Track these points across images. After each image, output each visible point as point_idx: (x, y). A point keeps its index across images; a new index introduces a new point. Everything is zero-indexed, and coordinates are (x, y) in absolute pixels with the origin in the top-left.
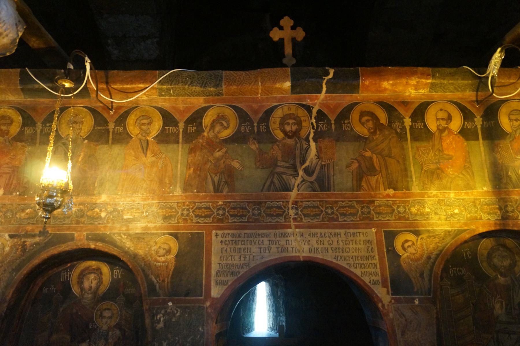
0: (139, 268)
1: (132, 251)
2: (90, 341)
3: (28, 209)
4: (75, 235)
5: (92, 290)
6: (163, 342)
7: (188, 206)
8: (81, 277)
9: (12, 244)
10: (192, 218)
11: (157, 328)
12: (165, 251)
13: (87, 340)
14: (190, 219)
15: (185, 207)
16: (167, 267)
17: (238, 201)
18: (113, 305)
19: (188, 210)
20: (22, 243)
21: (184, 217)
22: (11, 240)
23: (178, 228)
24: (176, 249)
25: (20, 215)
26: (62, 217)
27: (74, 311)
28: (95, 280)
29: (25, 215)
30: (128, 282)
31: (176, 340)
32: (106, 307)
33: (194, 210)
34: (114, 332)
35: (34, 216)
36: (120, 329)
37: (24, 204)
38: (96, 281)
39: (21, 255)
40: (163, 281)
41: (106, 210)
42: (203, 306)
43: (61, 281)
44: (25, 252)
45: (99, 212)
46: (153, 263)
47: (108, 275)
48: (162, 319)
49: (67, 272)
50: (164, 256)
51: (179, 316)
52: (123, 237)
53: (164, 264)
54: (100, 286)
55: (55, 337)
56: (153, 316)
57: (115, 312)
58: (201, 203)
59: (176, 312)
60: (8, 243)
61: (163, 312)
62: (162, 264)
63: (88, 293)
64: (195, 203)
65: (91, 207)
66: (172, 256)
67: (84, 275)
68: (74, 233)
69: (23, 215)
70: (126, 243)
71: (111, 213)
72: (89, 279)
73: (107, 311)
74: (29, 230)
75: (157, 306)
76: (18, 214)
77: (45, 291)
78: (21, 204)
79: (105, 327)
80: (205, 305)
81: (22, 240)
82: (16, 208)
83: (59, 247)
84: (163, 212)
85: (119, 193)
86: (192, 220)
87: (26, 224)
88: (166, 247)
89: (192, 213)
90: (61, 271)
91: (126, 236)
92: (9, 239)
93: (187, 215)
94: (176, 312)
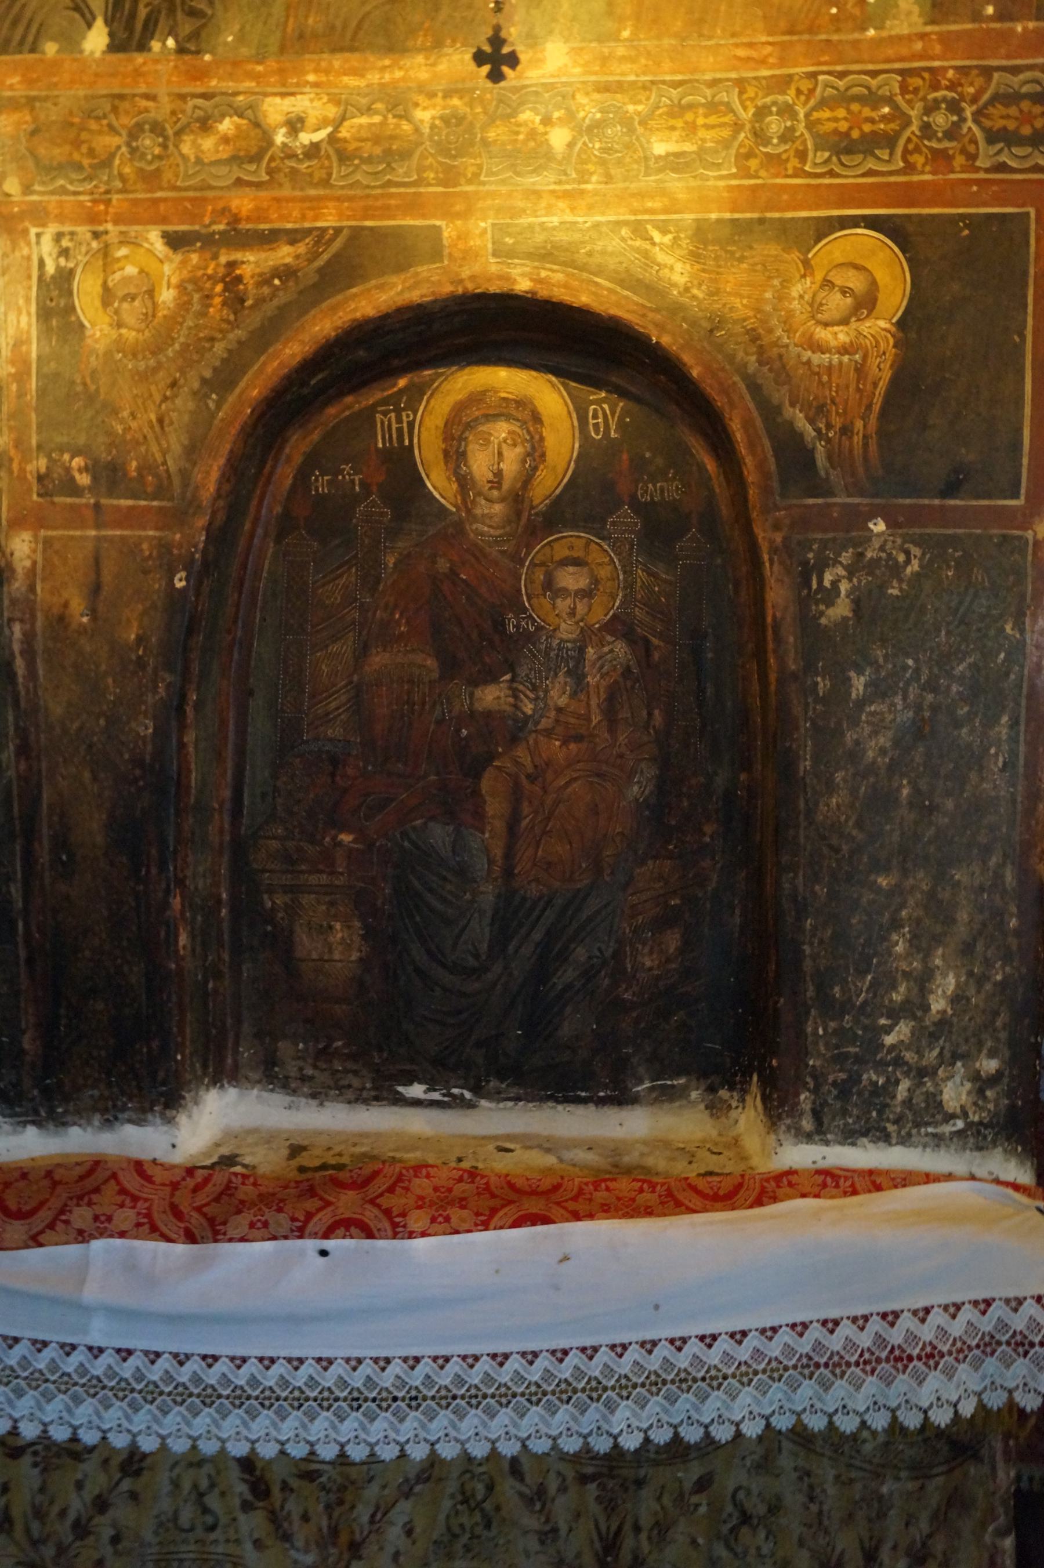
0: (736, 378)
1: (700, 302)
2: (513, 680)
3: (223, 116)
4: (445, 234)
5: (506, 485)
6: (852, 674)
7: (952, 86)
8: (456, 431)
9: (185, 274)
10: (972, 149)
11: (823, 621)
12: (849, 300)
13: (505, 674)
14: (963, 151)
15: (939, 94)
16: (860, 370)
17: (264, 511)
18: (593, 546)
19: (954, 107)
20: (222, 271)
21: (934, 144)
22: (178, 258)
23: (908, 194)
24: (899, 292)
25: (195, 145)
26: (378, 151)
27: (443, 565)
28: (515, 445)
29: (217, 145)
30: (648, 455)
31: (906, 668)
32: (566, 553)
33: (985, 106)
34: (606, 649)
35: (254, 150)
36: (629, 635)
37: (205, 96)
38: (519, 450)
39: (228, 322)
40: (846, 431)
41: (571, 115)
42: (1020, 538)
43: (377, 449)
44: (243, 307)
45: (541, 129)
46: (799, 356)
47: (567, 424)
48: (844, 587)
49: (398, 411)
50: (844, 322)
51: (917, 575)
52: (657, 236)
53: (846, 358)
54: (535, 469)
55: (378, 659)
56: (806, 573)
57: (604, 573)
58: (1015, 70)
59: (901, 558)
60: (167, 269)
61: (846, 557)
62: (836, 358)
63: (488, 500)
64: (987, 72)
65: (500, 101)
66: (882, 324)
67: (469, 426)
68: (438, 223)
69: (208, 143)
70: (672, 268)
71: (594, 128)
72: (487, 442)
73: (571, 569)
74: (244, 213)
75: (819, 536)
76: (188, 139)
77: (321, 484)
78: (195, 96)
79: (567, 631)
80: (1029, 534)
81: (223, 259)
82: (173, 113)
83: (381, 287)
84: (836, 120)
85: (626, 34)
86: (973, 157)
87: (228, 188)
88: (856, 282)
89: (976, 121)
90: (372, 409)
91: (670, 236)
92: (170, 252)
93: (951, 134)
94: (901, 558)
